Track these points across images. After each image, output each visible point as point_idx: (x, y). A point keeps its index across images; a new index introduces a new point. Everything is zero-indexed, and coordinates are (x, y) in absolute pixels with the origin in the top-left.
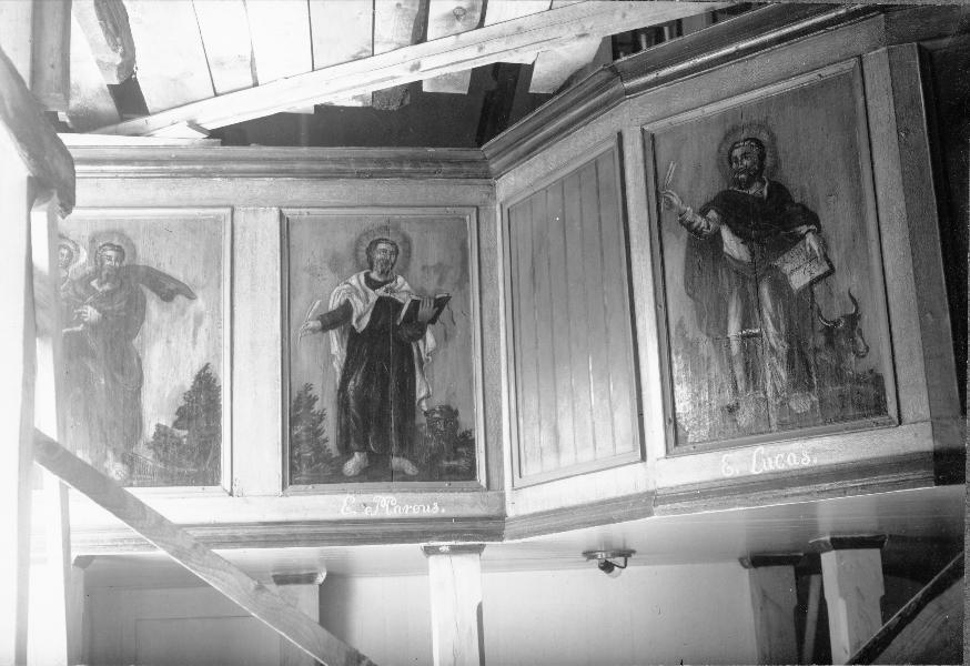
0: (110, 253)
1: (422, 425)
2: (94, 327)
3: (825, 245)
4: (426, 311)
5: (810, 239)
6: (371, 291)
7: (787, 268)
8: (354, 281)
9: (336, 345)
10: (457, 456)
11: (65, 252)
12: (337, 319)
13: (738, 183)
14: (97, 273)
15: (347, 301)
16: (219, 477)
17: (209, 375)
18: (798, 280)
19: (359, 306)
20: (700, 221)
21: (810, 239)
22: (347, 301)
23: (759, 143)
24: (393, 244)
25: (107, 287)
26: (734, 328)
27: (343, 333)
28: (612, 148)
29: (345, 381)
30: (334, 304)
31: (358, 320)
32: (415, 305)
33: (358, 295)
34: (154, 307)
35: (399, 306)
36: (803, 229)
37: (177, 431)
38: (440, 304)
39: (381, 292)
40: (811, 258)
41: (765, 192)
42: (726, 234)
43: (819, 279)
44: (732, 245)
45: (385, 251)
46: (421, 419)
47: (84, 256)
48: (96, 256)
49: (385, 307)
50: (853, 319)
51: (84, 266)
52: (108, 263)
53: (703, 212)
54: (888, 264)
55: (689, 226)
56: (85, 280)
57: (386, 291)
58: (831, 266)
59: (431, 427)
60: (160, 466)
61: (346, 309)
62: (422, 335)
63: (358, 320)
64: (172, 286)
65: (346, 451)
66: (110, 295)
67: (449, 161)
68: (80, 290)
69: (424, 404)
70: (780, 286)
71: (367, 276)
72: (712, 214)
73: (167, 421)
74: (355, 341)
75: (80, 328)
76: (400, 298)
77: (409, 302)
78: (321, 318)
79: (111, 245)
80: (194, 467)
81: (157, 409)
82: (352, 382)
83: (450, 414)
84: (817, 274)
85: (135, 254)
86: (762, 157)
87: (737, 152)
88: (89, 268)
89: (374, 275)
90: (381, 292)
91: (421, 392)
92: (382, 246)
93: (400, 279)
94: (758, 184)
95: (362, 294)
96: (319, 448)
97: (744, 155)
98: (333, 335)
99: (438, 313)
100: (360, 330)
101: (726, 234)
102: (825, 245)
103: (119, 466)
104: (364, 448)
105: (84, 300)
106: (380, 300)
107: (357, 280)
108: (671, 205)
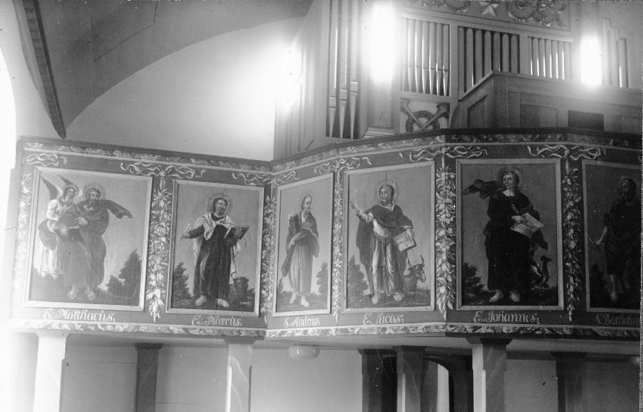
0: (94, 193)
1: (231, 285)
2: (83, 227)
3: (413, 234)
4: (237, 233)
5: (408, 231)
6: (213, 222)
7: (398, 242)
8: (206, 216)
9: (195, 245)
10: (246, 300)
11: (72, 190)
12: (197, 233)
13: (382, 203)
14: (87, 202)
15: (203, 225)
16: (139, 302)
17: (136, 254)
18: (402, 247)
19: (207, 228)
20: (364, 216)
21: (408, 231)
22: (203, 225)
23: (392, 188)
24: (226, 201)
25: (91, 209)
26: (375, 263)
27: (199, 241)
28: (330, 178)
29: (199, 263)
30: (197, 225)
31: (207, 234)
32: (233, 229)
33: (207, 222)
34: (112, 216)
35: (226, 230)
36: (406, 227)
37: (119, 279)
38: (244, 231)
39: (218, 222)
40: (408, 239)
41: (393, 209)
42: (375, 224)
43: (410, 248)
44: (377, 228)
45: (221, 204)
46: (231, 282)
47: (81, 193)
48: (87, 194)
49: (220, 230)
50: (421, 266)
51: (80, 198)
52: (92, 197)
53: (367, 213)
54: (347, 194)
55: (360, 217)
56: (81, 205)
57: (221, 222)
58: (415, 243)
59: (236, 286)
60: (111, 295)
61: (202, 229)
62: (235, 244)
63: (207, 234)
64: (122, 211)
65: (197, 296)
66: (92, 213)
67: (454, 281)
68: (78, 209)
69: (233, 275)
70: (395, 248)
71: (212, 214)
72: (371, 214)
73: (116, 275)
74: (204, 245)
75: (77, 227)
76: (226, 226)
77: (230, 228)
78: (190, 232)
79: (95, 189)
80: (157, 318)
81: (112, 267)
82: (202, 263)
83: (245, 281)
84: (410, 246)
85: (105, 195)
86: (393, 194)
87: (383, 190)
88: (83, 199)
89: (216, 214)
90: (218, 222)
91: (232, 270)
92: (220, 201)
93: (227, 217)
94: (389, 205)
95: (209, 222)
96: (185, 292)
97: (386, 192)
98: (195, 240)
99: (243, 234)
100: (207, 239)
101: (375, 224)
102: (413, 234)
103: (92, 293)
104: (205, 294)
105: (80, 214)
106: (218, 226)
107: (208, 216)
108: (353, 207)
